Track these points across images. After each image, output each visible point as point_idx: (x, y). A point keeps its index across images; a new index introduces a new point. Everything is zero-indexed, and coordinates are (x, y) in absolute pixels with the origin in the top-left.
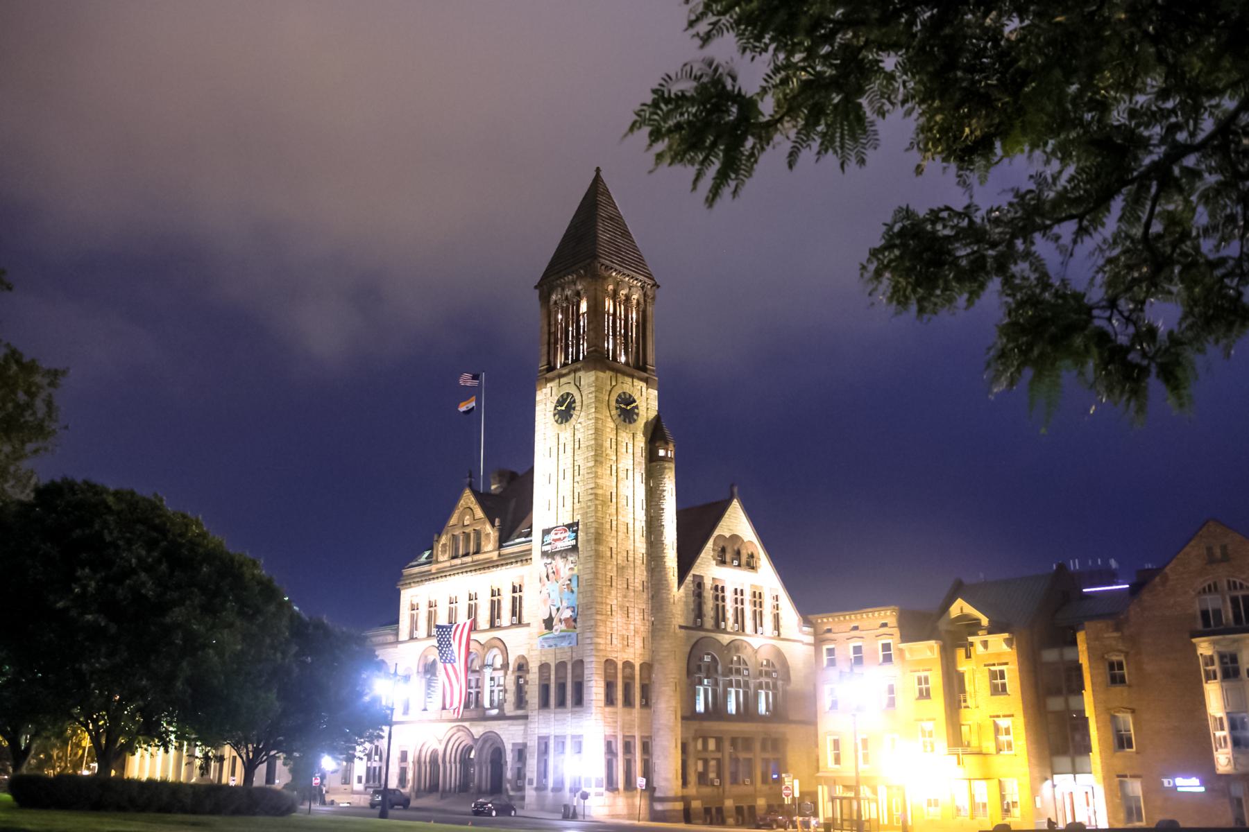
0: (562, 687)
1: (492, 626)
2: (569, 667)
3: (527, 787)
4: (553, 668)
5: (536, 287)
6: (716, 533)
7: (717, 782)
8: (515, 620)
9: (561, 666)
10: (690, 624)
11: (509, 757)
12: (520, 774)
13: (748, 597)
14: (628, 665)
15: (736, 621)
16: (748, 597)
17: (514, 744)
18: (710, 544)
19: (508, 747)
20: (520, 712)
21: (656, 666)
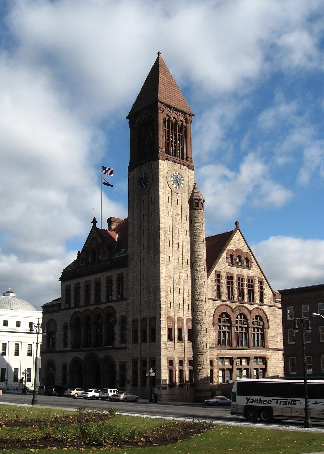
0: (144, 331)
1: (108, 301)
2: (148, 321)
3: (127, 384)
4: (140, 322)
5: (127, 118)
6: (228, 248)
9: (144, 320)
10: (214, 297)
11: (118, 369)
12: (123, 377)
13: (246, 282)
14: (179, 319)
15: (239, 296)
16: (246, 282)
18: (224, 255)
19: (117, 364)
20: (123, 345)
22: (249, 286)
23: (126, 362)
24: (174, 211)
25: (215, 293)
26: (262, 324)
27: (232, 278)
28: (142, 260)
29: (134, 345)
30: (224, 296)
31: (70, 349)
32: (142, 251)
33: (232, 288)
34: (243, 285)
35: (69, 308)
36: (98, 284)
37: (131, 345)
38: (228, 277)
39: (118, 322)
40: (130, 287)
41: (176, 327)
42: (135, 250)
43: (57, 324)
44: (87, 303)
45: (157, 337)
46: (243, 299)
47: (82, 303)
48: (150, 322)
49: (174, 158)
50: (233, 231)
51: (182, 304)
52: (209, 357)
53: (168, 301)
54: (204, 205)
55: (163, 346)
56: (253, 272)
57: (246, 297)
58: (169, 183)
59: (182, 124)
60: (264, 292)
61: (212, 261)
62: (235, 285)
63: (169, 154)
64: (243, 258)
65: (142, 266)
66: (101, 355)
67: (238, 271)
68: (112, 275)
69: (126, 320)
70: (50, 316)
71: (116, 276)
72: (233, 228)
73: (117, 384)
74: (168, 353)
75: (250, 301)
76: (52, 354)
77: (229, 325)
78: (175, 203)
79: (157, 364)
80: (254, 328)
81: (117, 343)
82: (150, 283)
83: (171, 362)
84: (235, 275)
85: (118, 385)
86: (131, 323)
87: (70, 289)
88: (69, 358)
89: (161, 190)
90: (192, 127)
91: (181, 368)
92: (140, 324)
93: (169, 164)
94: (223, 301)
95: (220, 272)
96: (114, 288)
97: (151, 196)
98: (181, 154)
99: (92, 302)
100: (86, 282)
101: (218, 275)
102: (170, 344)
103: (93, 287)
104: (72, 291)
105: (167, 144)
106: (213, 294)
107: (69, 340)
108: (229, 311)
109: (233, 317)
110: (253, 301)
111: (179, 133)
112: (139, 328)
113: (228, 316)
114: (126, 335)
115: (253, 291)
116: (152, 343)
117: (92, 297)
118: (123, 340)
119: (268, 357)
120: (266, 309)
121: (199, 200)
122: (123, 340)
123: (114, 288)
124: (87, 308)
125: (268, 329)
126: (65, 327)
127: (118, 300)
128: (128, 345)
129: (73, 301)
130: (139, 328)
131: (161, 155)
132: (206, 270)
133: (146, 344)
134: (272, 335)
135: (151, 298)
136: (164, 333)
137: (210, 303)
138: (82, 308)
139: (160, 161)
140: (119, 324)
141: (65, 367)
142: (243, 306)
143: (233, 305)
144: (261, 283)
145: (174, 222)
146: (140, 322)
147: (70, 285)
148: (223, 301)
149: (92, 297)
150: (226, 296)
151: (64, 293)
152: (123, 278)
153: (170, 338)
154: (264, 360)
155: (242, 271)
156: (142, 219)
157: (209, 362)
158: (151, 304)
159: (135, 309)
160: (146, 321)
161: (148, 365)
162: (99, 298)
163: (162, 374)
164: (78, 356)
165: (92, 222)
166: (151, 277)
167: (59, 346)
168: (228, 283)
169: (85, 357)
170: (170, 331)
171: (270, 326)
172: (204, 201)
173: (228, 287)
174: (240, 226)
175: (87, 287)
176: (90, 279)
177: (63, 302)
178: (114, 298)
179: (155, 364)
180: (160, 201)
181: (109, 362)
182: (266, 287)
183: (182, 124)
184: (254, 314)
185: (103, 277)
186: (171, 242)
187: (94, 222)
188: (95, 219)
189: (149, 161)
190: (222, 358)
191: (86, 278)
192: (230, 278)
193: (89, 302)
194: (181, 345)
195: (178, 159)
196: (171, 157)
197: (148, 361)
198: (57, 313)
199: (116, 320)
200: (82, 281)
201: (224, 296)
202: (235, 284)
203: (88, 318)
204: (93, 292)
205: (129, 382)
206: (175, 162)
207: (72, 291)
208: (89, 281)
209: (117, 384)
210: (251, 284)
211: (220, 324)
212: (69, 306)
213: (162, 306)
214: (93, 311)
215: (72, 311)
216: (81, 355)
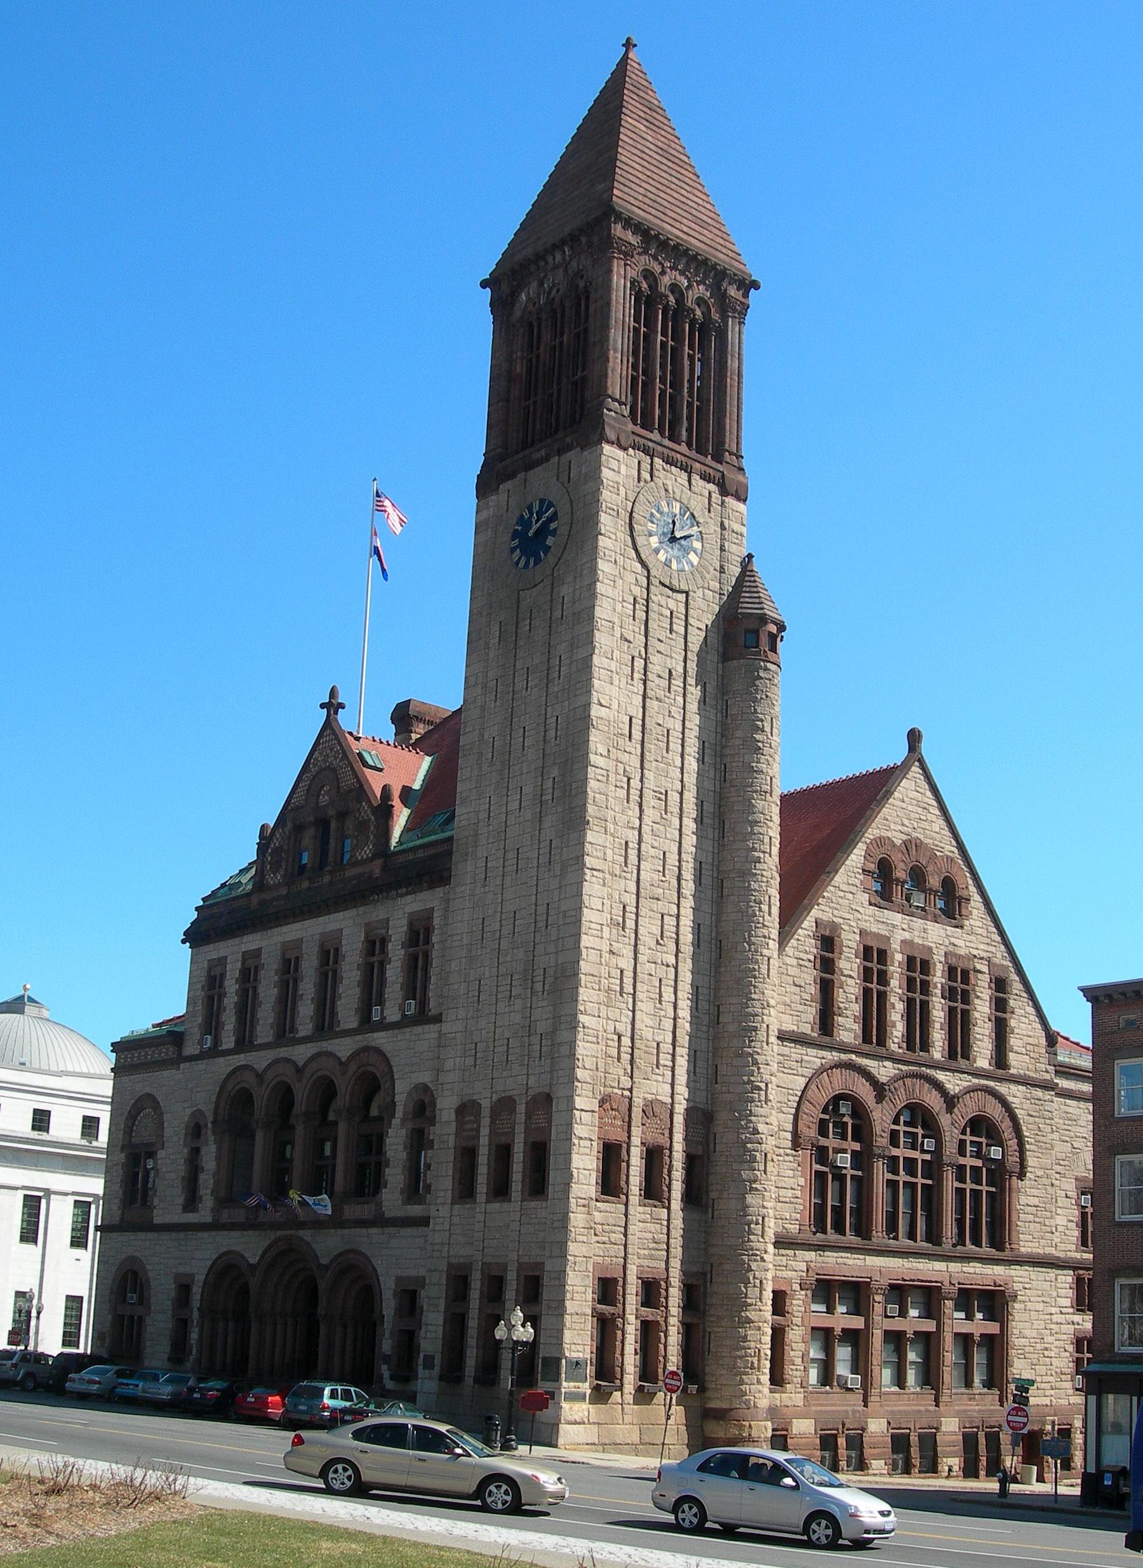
0: (503, 1153)
1: (367, 1023)
2: (521, 1109)
4: (486, 1113)
5: (484, 284)
7: (854, 1380)
8: (412, 1006)
9: (504, 1105)
11: (389, 1306)
12: (408, 1340)
13: (938, 978)
14: (650, 1109)
16: (938, 978)
17: (399, 1280)
18: (856, 857)
20: (416, 1210)
21: (722, 1116)
22: (950, 994)
23: (424, 1278)
24: (655, 658)
25: (811, 1013)
26: (995, 1153)
27: (883, 956)
28: (511, 855)
29: (456, 1207)
30: (848, 1028)
31: (209, 1219)
32: (511, 820)
33: (882, 996)
34: (925, 987)
35: (215, 1052)
36: (330, 956)
37: (444, 1211)
38: (867, 952)
39: (399, 1114)
40: (454, 965)
41: (636, 1140)
42: (483, 815)
43: (166, 1117)
44: (285, 1033)
45: (553, 1177)
46: (925, 1046)
47: (264, 1032)
48: (529, 1117)
49: (666, 442)
50: (894, 768)
51: (667, 1047)
52: (770, 1275)
53: (611, 1029)
54: (780, 645)
55: (577, 1219)
56: (970, 940)
57: (938, 1037)
58: (640, 541)
59: (707, 314)
60: (1013, 1023)
61: (803, 881)
62: (896, 984)
63: (647, 425)
64: (934, 882)
65: (508, 879)
66: (327, 1246)
67: (911, 929)
68: (388, 920)
69: (433, 1104)
70: (141, 1084)
71: (405, 922)
72: (897, 753)
73: (384, 1367)
74: (598, 1249)
75: (952, 1054)
76: (142, 1235)
77: (857, 1146)
78: (658, 628)
79: (546, 1294)
80: (961, 1169)
81: (391, 1198)
82: (540, 949)
83: (607, 1289)
84: (896, 945)
85: (386, 1374)
86: (453, 1117)
87: (223, 976)
88: (199, 1256)
89: (604, 567)
90: (745, 329)
91: (649, 1313)
92: (485, 1122)
93: (646, 466)
94: (843, 1048)
95: (835, 927)
96: (395, 973)
97: (565, 591)
98: (697, 423)
99: (305, 1028)
100: (286, 947)
101: (828, 942)
102: (611, 1210)
103: (309, 966)
104: (231, 986)
105: (641, 384)
106: (806, 1021)
107: (206, 1182)
108: (865, 1092)
109: (881, 1118)
110: (966, 1056)
111: (691, 347)
112: (484, 1140)
113: (859, 1111)
114: (428, 1167)
115: (966, 1014)
116: (533, 1204)
117: (306, 1010)
118: (415, 1189)
119: (1017, 1286)
120: (1015, 1094)
121: (763, 619)
122: (415, 1189)
123: (395, 973)
124: (283, 1052)
125: (1022, 1175)
126: (196, 1131)
127: (406, 1022)
128: (433, 1213)
129: (229, 1021)
130: (484, 1140)
131: (613, 427)
132: (775, 911)
133: (506, 1205)
134: (1035, 1201)
135: (537, 1014)
136: (585, 1164)
137: (786, 1051)
138: (262, 1053)
139: (607, 449)
140: (404, 1120)
141: (184, 1289)
142: (921, 1076)
143: (884, 1071)
144: (1000, 984)
145: (652, 704)
146: (486, 1113)
147: (222, 961)
148: (843, 1048)
149: (306, 1010)
150: (857, 1028)
151: (200, 994)
152: (429, 931)
153: (610, 1183)
154: (994, 1303)
155: (925, 930)
156: (520, 685)
157: (768, 1296)
158: (536, 1040)
159: (470, 1061)
160: (513, 1110)
161: (510, 1293)
162: (333, 1014)
163: (568, 1336)
164: (237, 1248)
165: (322, 706)
166: (542, 924)
167: (167, 1205)
168: (867, 974)
169: (265, 1253)
170: (612, 1155)
171: (1031, 1161)
172: (782, 628)
173: (867, 992)
174: (925, 748)
175: (290, 967)
176: (299, 935)
177: (194, 1032)
178: (392, 1014)
179: (538, 1291)
180: (599, 612)
181: (357, 1276)
182: (1018, 1003)
183: (707, 314)
184: (968, 1108)
185: (348, 926)
186: (635, 783)
187: (332, 706)
188: (333, 693)
189: (560, 453)
190: (825, 1290)
191: (285, 929)
192: (874, 956)
193: (293, 1029)
194: (656, 1220)
195: (683, 448)
196: (655, 436)
197: (511, 1276)
198: (166, 1073)
199: (394, 1103)
200: (269, 943)
201: (848, 1028)
202: (894, 983)
203: (285, 1096)
204: (308, 988)
205: (429, 1362)
206: (669, 461)
207: (231, 986)
208: (298, 944)
209: (384, 1367)
210: (959, 985)
211: (823, 1142)
212: (216, 1041)
213: (584, 1049)
214: (306, 1065)
215: (222, 1066)
216: (251, 1247)
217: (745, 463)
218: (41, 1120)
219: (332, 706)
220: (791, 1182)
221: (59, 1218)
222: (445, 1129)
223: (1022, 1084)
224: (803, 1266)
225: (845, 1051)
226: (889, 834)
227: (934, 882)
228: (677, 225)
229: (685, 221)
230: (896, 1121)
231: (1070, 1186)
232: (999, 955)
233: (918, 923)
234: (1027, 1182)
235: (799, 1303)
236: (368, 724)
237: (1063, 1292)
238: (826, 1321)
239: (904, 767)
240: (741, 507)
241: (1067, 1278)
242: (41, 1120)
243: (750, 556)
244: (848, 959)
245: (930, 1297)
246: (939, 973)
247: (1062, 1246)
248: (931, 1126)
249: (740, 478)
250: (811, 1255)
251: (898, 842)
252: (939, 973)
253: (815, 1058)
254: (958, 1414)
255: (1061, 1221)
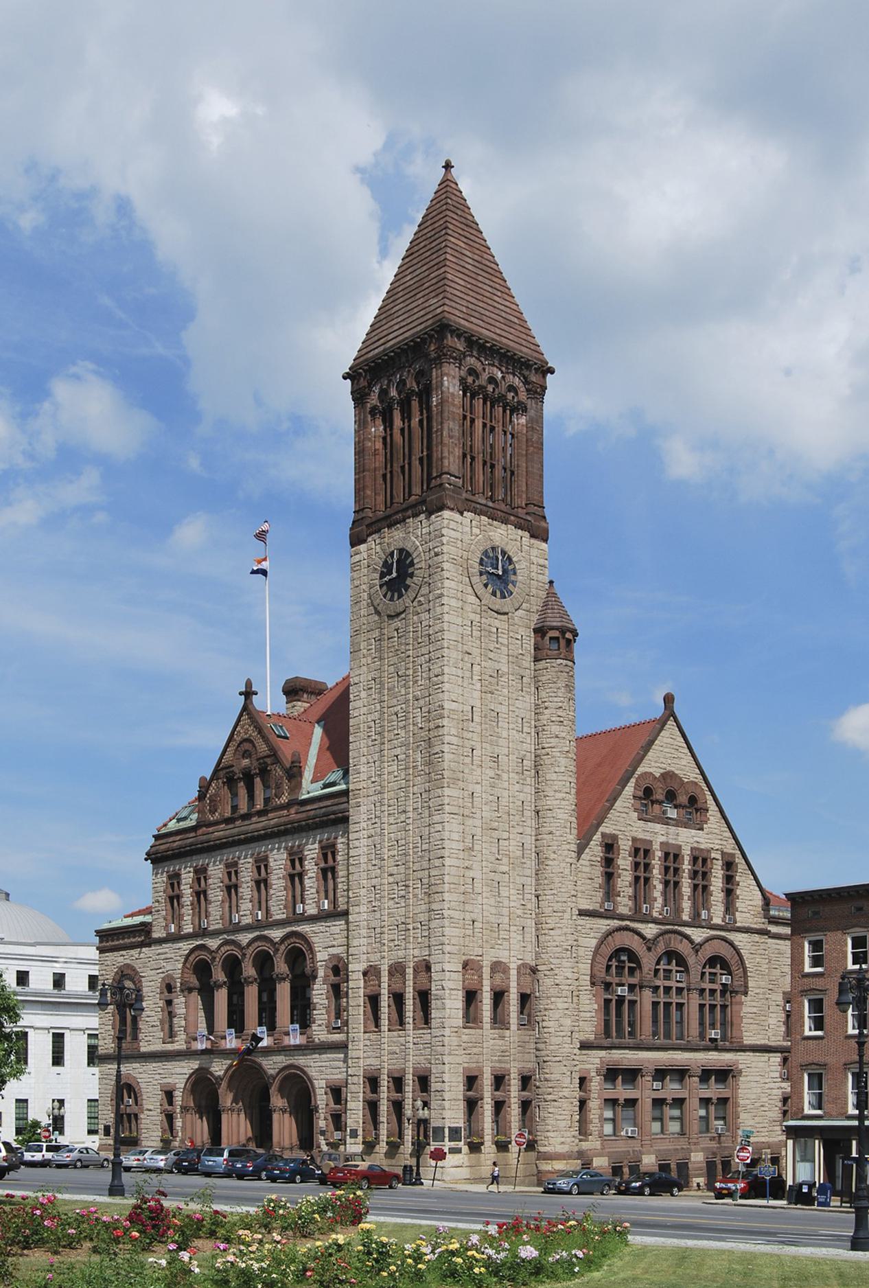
9: (397, 970)
16: (686, 866)
56: (708, 837)
64: (683, 799)
74: (466, 1058)
80: (702, 991)
84: (656, 846)
94: (622, 918)
95: (615, 837)
101: (610, 846)
112: (385, 992)
113: (633, 957)
119: (741, 1067)
120: (738, 939)
134: (755, 1010)
144: (729, 865)
148: (622, 918)
165: (241, 694)
168: (636, 865)
184: (708, 952)
190: (611, 1074)
201: (624, 905)
202: (655, 871)
211: (609, 979)
217: (547, 512)
218: (59, 981)
219: (248, 694)
220: (588, 1008)
221: (76, 1048)
222: (357, 986)
223: (746, 932)
224: (598, 1061)
225: (623, 920)
226: (651, 770)
227: (683, 799)
228: (492, 329)
229: (497, 324)
230: (658, 963)
231: (780, 998)
232: (730, 847)
233: (672, 829)
234: (749, 998)
235: (596, 1083)
236: (270, 701)
237: (773, 1068)
238: (611, 1094)
239: (662, 723)
240: (544, 546)
241: (776, 1058)
242: (59, 981)
243: (551, 582)
244: (624, 858)
245: (681, 1074)
246: (686, 862)
247: (773, 1038)
248: (682, 962)
249: (543, 524)
250: (603, 1053)
251: (658, 775)
252: (686, 862)
253: (604, 925)
254: (703, 1150)
255: (771, 1021)
